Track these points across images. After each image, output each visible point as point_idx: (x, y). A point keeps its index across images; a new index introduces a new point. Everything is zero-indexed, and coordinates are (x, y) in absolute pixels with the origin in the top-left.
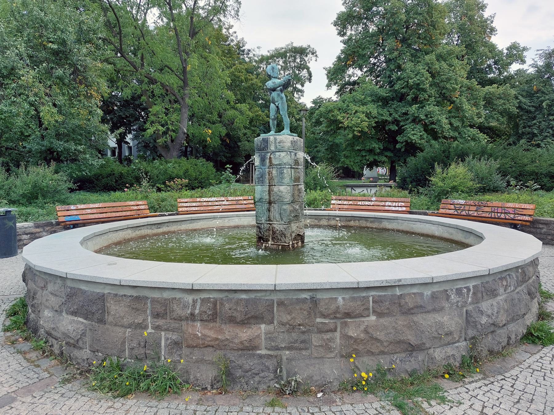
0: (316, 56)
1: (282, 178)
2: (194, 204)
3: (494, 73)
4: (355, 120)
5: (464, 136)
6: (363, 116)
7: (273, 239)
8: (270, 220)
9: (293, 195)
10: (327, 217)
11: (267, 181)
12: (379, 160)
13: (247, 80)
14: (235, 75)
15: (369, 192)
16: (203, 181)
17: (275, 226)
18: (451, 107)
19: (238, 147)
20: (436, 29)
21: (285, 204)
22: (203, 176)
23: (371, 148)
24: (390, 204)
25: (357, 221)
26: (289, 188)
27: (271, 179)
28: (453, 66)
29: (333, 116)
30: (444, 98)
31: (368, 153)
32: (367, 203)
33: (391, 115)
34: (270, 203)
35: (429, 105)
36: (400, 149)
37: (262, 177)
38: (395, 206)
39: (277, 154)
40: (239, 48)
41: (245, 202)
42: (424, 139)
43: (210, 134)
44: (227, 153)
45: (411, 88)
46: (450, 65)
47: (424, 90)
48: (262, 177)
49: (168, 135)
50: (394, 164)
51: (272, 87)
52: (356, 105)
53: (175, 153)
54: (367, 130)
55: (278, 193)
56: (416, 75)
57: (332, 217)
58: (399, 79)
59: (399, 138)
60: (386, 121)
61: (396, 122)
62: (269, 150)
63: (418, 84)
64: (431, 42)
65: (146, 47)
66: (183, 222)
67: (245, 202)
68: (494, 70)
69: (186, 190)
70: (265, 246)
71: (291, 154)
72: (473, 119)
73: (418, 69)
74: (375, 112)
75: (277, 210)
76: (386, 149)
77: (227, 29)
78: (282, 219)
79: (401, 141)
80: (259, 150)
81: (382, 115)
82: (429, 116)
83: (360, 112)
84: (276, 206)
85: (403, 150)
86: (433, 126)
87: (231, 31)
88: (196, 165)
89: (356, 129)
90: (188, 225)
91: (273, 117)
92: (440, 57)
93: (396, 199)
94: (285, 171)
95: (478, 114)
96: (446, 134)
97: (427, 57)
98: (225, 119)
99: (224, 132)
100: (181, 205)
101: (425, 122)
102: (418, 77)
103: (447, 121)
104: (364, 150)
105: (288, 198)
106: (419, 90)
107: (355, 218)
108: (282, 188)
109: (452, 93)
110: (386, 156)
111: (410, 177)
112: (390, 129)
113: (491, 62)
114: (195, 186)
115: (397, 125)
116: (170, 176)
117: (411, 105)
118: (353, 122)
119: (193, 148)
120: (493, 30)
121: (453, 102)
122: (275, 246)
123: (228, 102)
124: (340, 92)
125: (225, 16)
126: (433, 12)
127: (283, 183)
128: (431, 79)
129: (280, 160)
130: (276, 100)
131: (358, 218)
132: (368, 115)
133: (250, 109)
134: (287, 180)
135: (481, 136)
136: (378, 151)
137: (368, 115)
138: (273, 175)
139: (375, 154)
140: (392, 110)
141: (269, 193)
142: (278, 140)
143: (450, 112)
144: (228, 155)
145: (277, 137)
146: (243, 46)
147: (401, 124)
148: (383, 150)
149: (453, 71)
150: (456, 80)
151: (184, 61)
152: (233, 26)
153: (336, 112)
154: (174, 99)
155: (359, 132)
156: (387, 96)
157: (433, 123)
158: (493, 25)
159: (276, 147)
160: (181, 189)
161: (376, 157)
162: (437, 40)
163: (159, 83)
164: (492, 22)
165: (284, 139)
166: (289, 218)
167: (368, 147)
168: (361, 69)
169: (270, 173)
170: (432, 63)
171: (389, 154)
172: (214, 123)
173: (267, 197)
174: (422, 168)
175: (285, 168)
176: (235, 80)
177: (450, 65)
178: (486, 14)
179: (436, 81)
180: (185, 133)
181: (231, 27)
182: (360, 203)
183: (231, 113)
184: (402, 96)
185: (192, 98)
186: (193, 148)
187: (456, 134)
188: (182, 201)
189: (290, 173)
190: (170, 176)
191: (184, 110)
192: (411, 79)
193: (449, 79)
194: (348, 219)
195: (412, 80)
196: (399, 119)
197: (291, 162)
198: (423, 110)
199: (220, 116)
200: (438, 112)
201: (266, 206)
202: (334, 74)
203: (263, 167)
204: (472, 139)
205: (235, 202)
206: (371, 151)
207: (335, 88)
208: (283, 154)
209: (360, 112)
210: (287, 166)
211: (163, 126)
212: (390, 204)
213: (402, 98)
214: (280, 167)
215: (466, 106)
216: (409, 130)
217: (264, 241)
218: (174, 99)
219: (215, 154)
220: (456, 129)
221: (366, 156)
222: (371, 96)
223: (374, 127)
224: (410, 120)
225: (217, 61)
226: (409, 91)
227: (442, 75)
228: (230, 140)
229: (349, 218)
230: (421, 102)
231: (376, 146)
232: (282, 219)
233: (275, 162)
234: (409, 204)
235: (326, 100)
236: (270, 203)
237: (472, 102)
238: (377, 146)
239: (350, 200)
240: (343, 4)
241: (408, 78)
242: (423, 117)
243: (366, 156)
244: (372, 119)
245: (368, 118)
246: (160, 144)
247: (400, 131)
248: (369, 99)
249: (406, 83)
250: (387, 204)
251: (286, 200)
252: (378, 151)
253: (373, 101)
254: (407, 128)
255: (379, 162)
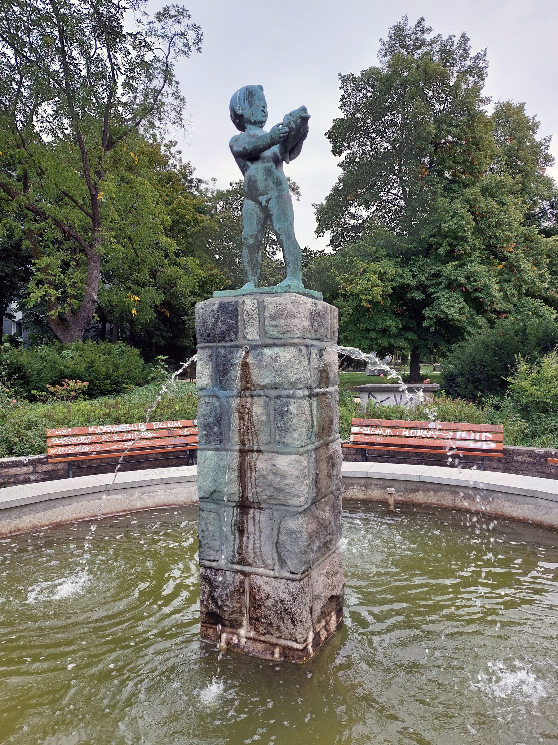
0: (298, 193)
1: (284, 430)
2: (82, 439)
3: (550, 220)
4: (362, 285)
5: (522, 309)
6: (374, 278)
7: (254, 621)
8: (243, 561)
9: (316, 482)
10: (363, 482)
11: (236, 438)
12: (396, 345)
13: (196, 222)
14: (177, 213)
15: (398, 400)
16: (120, 380)
17: (259, 581)
18: (502, 266)
19: (184, 323)
20: (479, 150)
21: (295, 515)
22: (121, 371)
23: (384, 327)
24: (464, 435)
25: (432, 493)
26: (304, 461)
27: (247, 431)
28: (504, 204)
29: (328, 277)
30: (493, 252)
31: (380, 335)
32: (419, 433)
33: (414, 276)
34: (244, 506)
35: (472, 262)
36: (428, 329)
37: (218, 422)
38: (475, 440)
39: (269, 352)
40: (185, 177)
41: (186, 432)
42: (464, 314)
43: (139, 303)
44: (167, 332)
45: (445, 236)
46: (502, 204)
47: (464, 239)
48: (218, 422)
49: (66, 305)
50: (418, 352)
51: (249, 147)
52: (363, 261)
53: (78, 334)
54: (380, 299)
55: (270, 477)
56: (452, 216)
57: (375, 482)
58: (424, 222)
59: (426, 312)
60: (408, 285)
61: (422, 288)
62: (241, 341)
63: (455, 232)
64: (473, 171)
65: (29, 160)
66: (26, 509)
67: (186, 432)
68: (550, 216)
69: (85, 400)
70: (228, 643)
71: (309, 354)
72: (533, 283)
73: (454, 207)
74: (392, 272)
75: (266, 532)
76: (406, 328)
77: (168, 146)
78: (282, 562)
79: (431, 316)
80: (210, 338)
81: (402, 277)
82: (472, 279)
83: (370, 271)
84: (263, 517)
85: (432, 329)
86: (478, 294)
87: (173, 150)
88: (109, 353)
89: (364, 297)
90: (41, 515)
91: (251, 241)
92: (486, 191)
93: (475, 426)
94: (293, 408)
95: (541, 276)
96: (497, 307)
97: (467, 191)
98: (161, 281)
99: (158, 297)
100: (53, 441)
101: (466, 289)
102: (455, 220)
103: (497, 287)
104: (375, 329)
105: (302, 494)
106: (456, 239)
107: (427, 486)
108: (283, 462)
109: (505, 245)
110: (406, 339)
111: (463, 375)
112: (413, 299)
113: (545, 204)
114: (106, 390)
115: (424, 292)
116: (62, 374)
117: (445, 263)
118: (359, 287)
119: (108, 324)
120: (548, 159)
121: (505, 259)
122: (261, 646)
123: (167, 256)
124: (334, 242)
125: (160, 119)
126: (476, 124)
127: (287, 445)
128: (474, 223)
129: (278, 371)
130: (261, 186)
131: (433, 486)
132: (383, 276)
133: (201, 266)
134: (299, 435)
135: (546, 309)
136: (395, 331)
137: (383, 276)
138: (255, 419)
139: (390, 336)
140: (416, 270)
141: (242, 477)
142: (271, 309)
143: (501, 273)
144: (168, 335)
145: (268, 299)
146: (191, 173)
147: (430, 290)
148: (402, 329)
149: (505, 212)
150: (509, 225)
151: (94, 189)
152: (176, 143)
153: (334, 271)
154: (75, 245)
155: (369, 301)
156: (409, 249)
157: (476, 290)
158: (549, 152)
159: (263, 331)
160: (76, 398)
161: (392, 341)
162: (480, 165)
163: (50, 220)
164: (546, 148)
165: (290, 306)
166: (305, 558)
167: (380, 326)
168: (367, 207)
169: (244, 412)
170: (475, 200)
171: (410, 335)
172: (144, 285)
173: (234, 488)
174: (482, 360)
175: (293, 397)
176: (177, 222)
177: (502, 204)
178: (538, 137)
179: (480, 226)
180: (94, 301)
181: (173, 144)
182: (406, 433)
183: (170, 270)
184: (434, 247)
185: (105, 242)
186: (108, 324)
187: (511, 307)
188: (56, 433)
189: (308, 412)
190: (62, 374)
191: (93, 264)
192: (445, 222)
193: (499, 225)
194: (409, 486)
195: (447, 225)
196: (427, 283)
197: (310, 377)
198: (463, 270)
199: (153, 274)
200: (485, 274)
201: (230, 515)
202: (328, 212)
203: (221, 393)
204: (533, 314)
205: (165, 433)
206: (384, 332)
207: (328, 235)
208: (286, 354)
209: (370, 271)
210: (300, 393)
211: (56, 288)
212: (464, 435)
213: (428, 250)
214: (275, 393)
215: (525, 264)
216: (442, 299)
217: (224, 625)
218: (75, 245)
219: (149, 334)
220: (506, 298)
221: (377, 339)
222: (385, 247)
223: (389, 295)
224: (443, 285)
225: (149, 191)
226: (441, 241)
227: (489, 218)
228: (172, 313)
229: (413, 486)
230: (459, 258)
231: (393, 324)
232: (282, 562)
233: (260, 377)
234: (500, 437)
235: (316, 253)
236: (244, 506)
237: (532, 259)
238: (393, 324)
239: (388, 427)
240: (341, 107)
241: (440, 220)
242: (463, 281)
243: (377, 339)
244: (387, 283)
245: (382, 281)
246: (54, 318)
247: (429, 301)
248: (383, 252)
249: (437, 229)
250: (459, 435)
251: (295, 501)
252: (395, 331)
253: (388, 255)
254: (438, 298)
255: (396, 348)
